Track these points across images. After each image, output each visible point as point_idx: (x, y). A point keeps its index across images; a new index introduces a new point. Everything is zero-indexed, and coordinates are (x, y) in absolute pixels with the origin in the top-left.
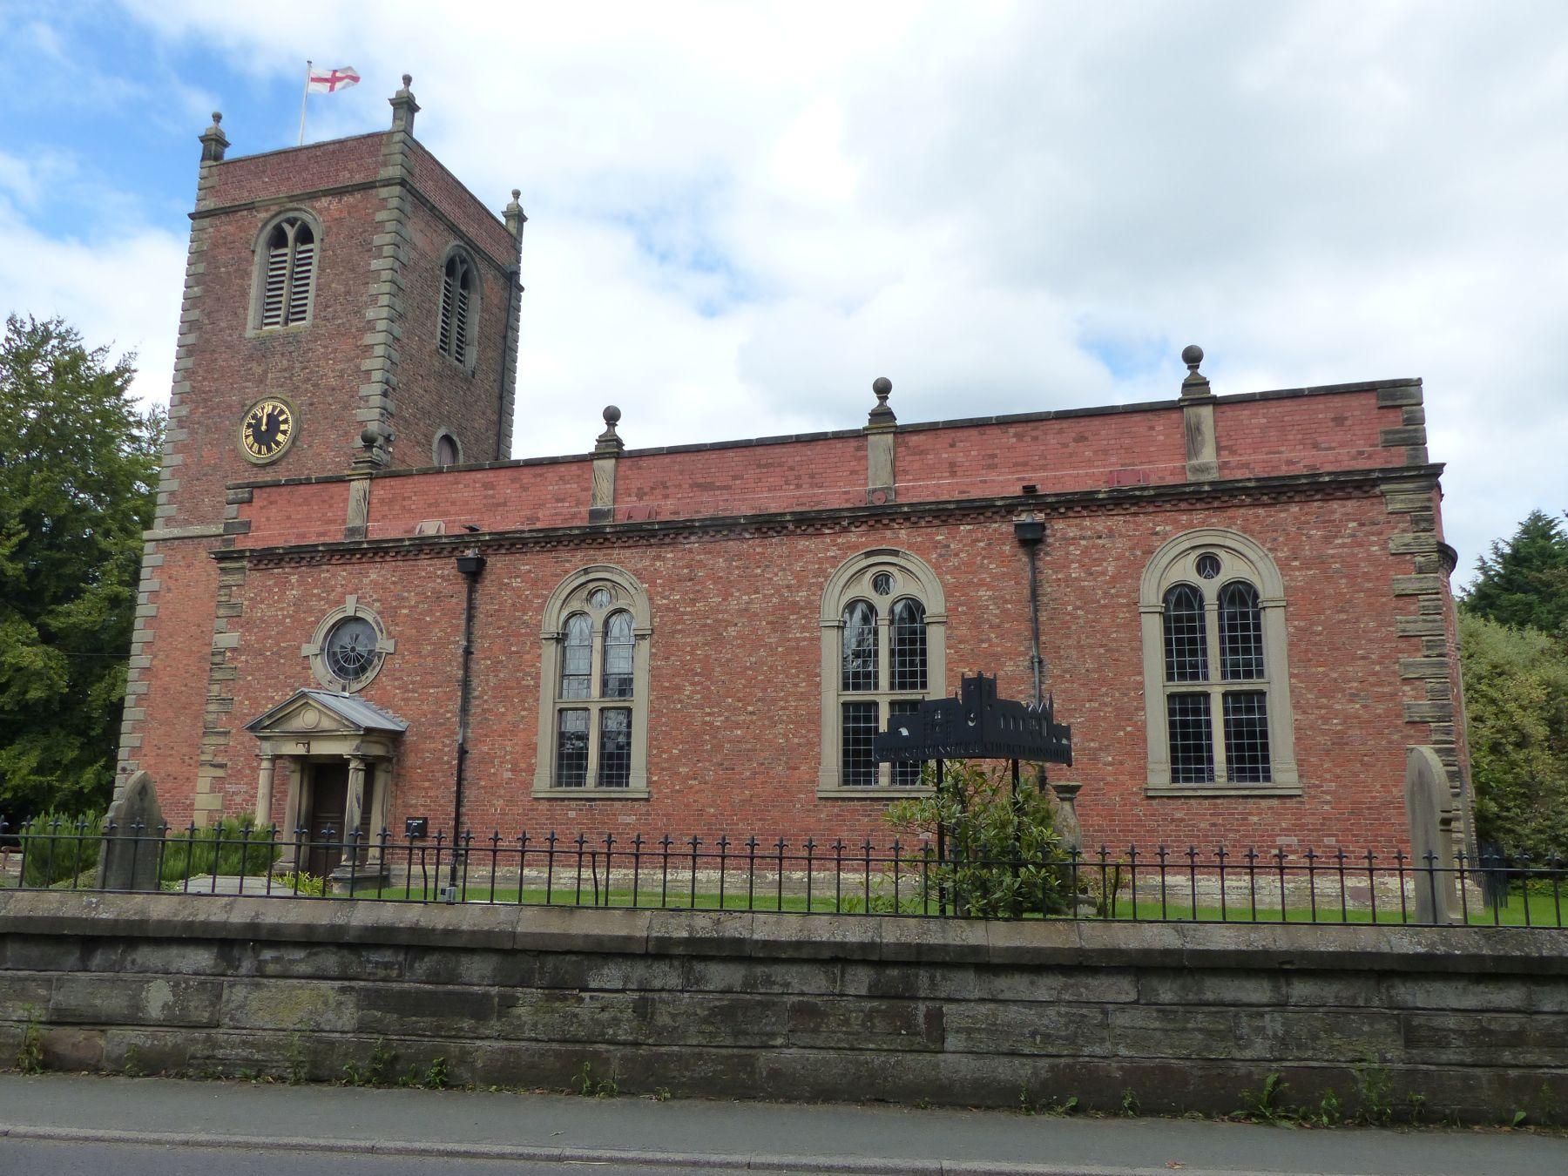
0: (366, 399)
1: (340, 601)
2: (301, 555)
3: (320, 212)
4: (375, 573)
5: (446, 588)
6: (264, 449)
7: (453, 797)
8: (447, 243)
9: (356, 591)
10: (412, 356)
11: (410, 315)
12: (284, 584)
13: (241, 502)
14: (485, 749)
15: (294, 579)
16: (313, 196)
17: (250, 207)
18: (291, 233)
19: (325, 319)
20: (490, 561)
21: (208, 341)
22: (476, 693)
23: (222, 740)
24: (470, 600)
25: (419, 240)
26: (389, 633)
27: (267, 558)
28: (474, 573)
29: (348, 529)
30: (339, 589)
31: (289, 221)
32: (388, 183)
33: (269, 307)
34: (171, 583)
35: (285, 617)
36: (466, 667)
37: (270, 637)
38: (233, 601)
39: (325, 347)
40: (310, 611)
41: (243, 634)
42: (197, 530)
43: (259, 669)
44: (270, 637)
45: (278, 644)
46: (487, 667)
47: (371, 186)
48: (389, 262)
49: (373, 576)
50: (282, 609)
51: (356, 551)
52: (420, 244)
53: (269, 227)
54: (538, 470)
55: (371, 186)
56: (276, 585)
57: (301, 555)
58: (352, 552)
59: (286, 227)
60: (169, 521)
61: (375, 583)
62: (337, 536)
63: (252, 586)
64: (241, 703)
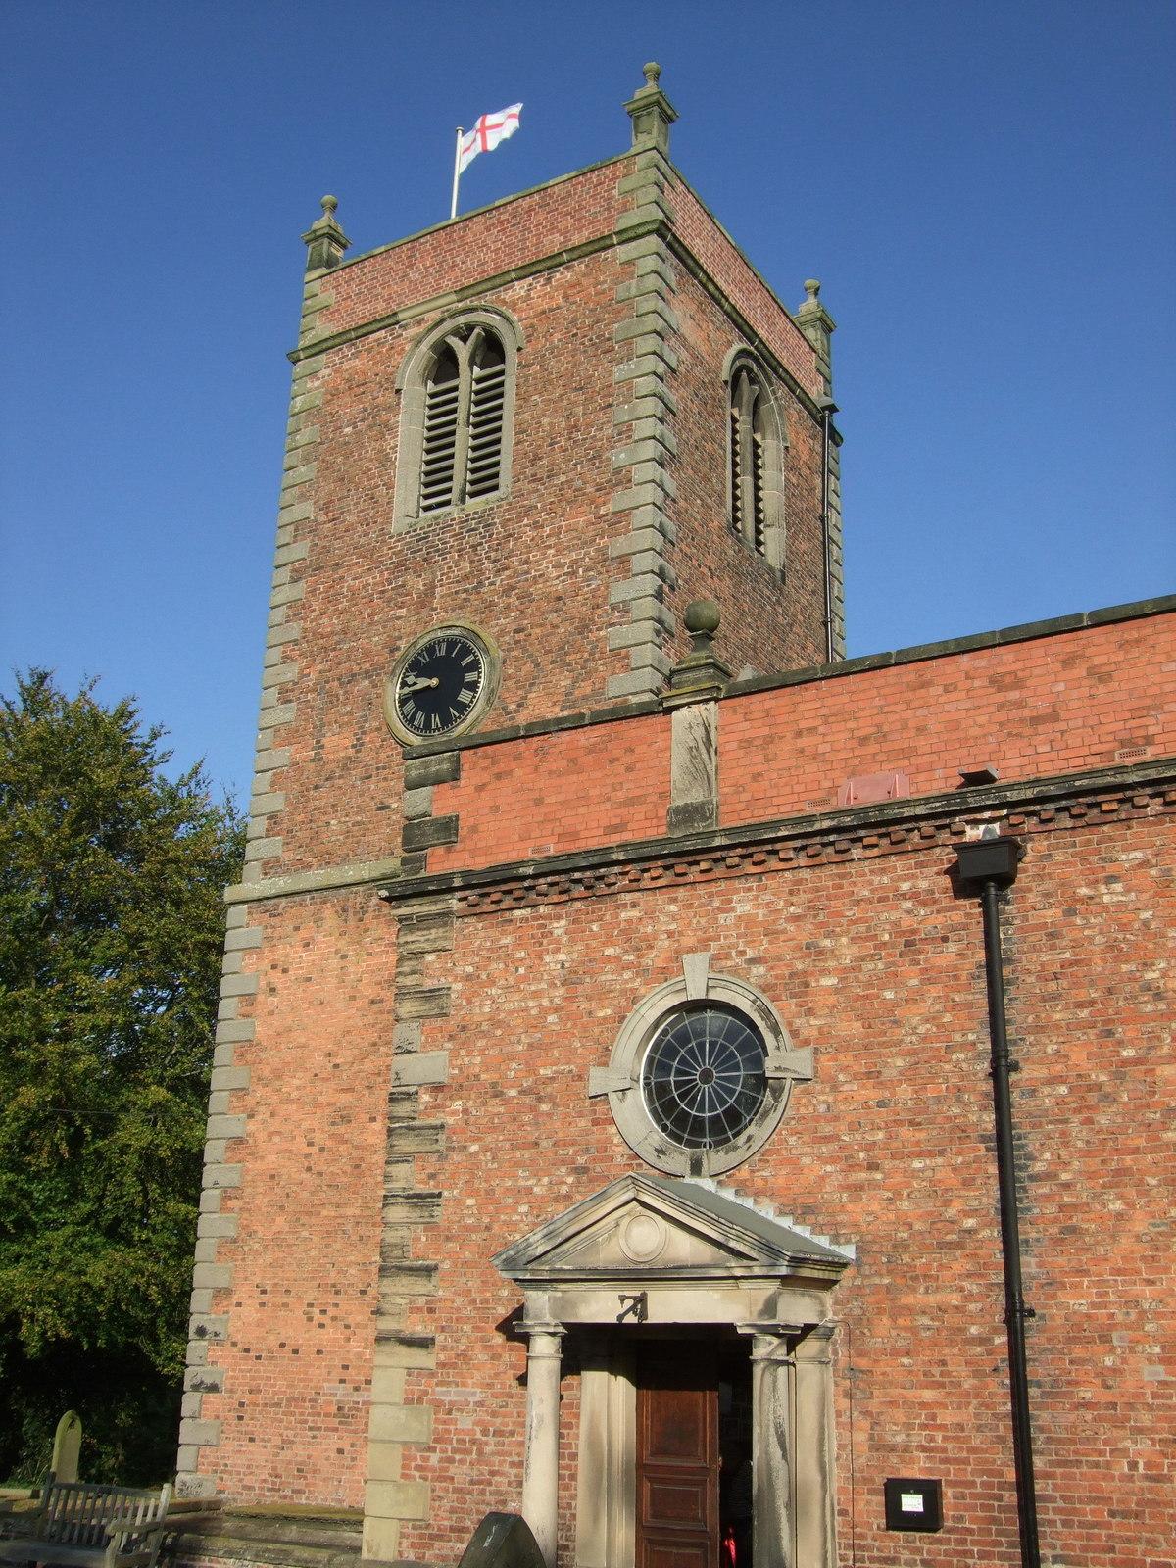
0: (624, 608)
1: (668, 972)
2: (579, 875)
3: (513, 306)
4: (747, 901)
5: (930, 920)
6: (436, 720)
7: (1005, 1429)
8: (730, 344)
9: (703, 944)
10: (693, 530)
11: (685, 458)
12: (541, 941)
13: (438, 781)
14: (1080, 1304)
15: (559, 927)
16: (499, 280)
17: (389, 321)
18: (463, 351)
19: (535, 479)
20: (1033, 849)
21: (327, 550)
22: (1038, 1167)
23: (421, 1286)
24: (990, 943)
25: (687, 329)
26: (794, 1033)
27: (499, 886)
28: (984, 878)
29: (677, 811)
30: (664, 942)
31: (456, 332)
32: (629, 236)
33: (436, 478)
34: (276, 978)
35: (544, 1012)
36: (1001, 1102)
37: (513, 1056)
38: (429, 984)
39: (537, 526)
40: (601, 994)
41: (454, 1054)
42: (316, 877)
43: (493, 1129)
44: (513, 1056)
45: (532, 1070)
46: (1060, 1102)
47: (601, 244)
48: (651, 363)
49: (743, 908)
50: (536, 995)
51: (693, 852)
52: (691, 340)
53: (425, 347)
54: (1130, 631)
55: (601, 244)
56: (519, 944)
57: (579, 875)
58: (691, 856)
59: (454, 342)
60: (270, 867)
61: (747, 921)
62: (647, 827)
63: (469, 951)
64: (459, 1202)
